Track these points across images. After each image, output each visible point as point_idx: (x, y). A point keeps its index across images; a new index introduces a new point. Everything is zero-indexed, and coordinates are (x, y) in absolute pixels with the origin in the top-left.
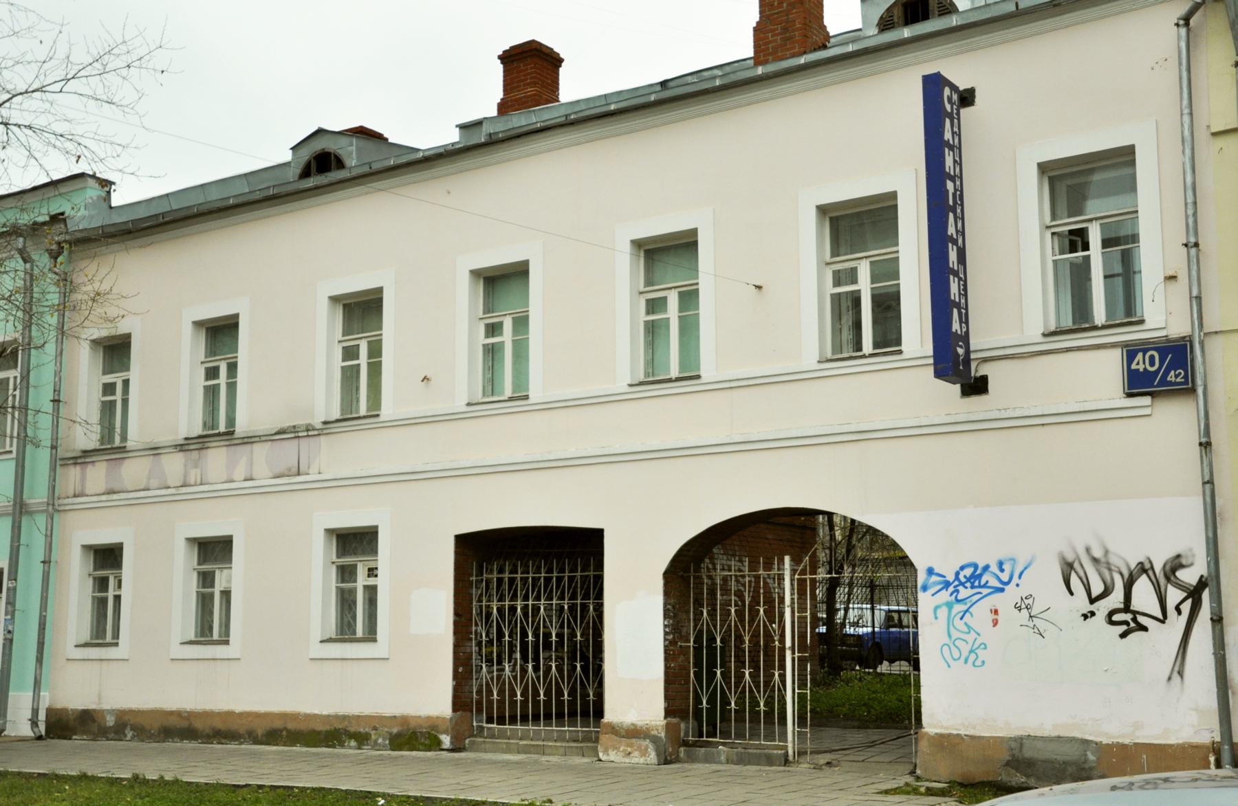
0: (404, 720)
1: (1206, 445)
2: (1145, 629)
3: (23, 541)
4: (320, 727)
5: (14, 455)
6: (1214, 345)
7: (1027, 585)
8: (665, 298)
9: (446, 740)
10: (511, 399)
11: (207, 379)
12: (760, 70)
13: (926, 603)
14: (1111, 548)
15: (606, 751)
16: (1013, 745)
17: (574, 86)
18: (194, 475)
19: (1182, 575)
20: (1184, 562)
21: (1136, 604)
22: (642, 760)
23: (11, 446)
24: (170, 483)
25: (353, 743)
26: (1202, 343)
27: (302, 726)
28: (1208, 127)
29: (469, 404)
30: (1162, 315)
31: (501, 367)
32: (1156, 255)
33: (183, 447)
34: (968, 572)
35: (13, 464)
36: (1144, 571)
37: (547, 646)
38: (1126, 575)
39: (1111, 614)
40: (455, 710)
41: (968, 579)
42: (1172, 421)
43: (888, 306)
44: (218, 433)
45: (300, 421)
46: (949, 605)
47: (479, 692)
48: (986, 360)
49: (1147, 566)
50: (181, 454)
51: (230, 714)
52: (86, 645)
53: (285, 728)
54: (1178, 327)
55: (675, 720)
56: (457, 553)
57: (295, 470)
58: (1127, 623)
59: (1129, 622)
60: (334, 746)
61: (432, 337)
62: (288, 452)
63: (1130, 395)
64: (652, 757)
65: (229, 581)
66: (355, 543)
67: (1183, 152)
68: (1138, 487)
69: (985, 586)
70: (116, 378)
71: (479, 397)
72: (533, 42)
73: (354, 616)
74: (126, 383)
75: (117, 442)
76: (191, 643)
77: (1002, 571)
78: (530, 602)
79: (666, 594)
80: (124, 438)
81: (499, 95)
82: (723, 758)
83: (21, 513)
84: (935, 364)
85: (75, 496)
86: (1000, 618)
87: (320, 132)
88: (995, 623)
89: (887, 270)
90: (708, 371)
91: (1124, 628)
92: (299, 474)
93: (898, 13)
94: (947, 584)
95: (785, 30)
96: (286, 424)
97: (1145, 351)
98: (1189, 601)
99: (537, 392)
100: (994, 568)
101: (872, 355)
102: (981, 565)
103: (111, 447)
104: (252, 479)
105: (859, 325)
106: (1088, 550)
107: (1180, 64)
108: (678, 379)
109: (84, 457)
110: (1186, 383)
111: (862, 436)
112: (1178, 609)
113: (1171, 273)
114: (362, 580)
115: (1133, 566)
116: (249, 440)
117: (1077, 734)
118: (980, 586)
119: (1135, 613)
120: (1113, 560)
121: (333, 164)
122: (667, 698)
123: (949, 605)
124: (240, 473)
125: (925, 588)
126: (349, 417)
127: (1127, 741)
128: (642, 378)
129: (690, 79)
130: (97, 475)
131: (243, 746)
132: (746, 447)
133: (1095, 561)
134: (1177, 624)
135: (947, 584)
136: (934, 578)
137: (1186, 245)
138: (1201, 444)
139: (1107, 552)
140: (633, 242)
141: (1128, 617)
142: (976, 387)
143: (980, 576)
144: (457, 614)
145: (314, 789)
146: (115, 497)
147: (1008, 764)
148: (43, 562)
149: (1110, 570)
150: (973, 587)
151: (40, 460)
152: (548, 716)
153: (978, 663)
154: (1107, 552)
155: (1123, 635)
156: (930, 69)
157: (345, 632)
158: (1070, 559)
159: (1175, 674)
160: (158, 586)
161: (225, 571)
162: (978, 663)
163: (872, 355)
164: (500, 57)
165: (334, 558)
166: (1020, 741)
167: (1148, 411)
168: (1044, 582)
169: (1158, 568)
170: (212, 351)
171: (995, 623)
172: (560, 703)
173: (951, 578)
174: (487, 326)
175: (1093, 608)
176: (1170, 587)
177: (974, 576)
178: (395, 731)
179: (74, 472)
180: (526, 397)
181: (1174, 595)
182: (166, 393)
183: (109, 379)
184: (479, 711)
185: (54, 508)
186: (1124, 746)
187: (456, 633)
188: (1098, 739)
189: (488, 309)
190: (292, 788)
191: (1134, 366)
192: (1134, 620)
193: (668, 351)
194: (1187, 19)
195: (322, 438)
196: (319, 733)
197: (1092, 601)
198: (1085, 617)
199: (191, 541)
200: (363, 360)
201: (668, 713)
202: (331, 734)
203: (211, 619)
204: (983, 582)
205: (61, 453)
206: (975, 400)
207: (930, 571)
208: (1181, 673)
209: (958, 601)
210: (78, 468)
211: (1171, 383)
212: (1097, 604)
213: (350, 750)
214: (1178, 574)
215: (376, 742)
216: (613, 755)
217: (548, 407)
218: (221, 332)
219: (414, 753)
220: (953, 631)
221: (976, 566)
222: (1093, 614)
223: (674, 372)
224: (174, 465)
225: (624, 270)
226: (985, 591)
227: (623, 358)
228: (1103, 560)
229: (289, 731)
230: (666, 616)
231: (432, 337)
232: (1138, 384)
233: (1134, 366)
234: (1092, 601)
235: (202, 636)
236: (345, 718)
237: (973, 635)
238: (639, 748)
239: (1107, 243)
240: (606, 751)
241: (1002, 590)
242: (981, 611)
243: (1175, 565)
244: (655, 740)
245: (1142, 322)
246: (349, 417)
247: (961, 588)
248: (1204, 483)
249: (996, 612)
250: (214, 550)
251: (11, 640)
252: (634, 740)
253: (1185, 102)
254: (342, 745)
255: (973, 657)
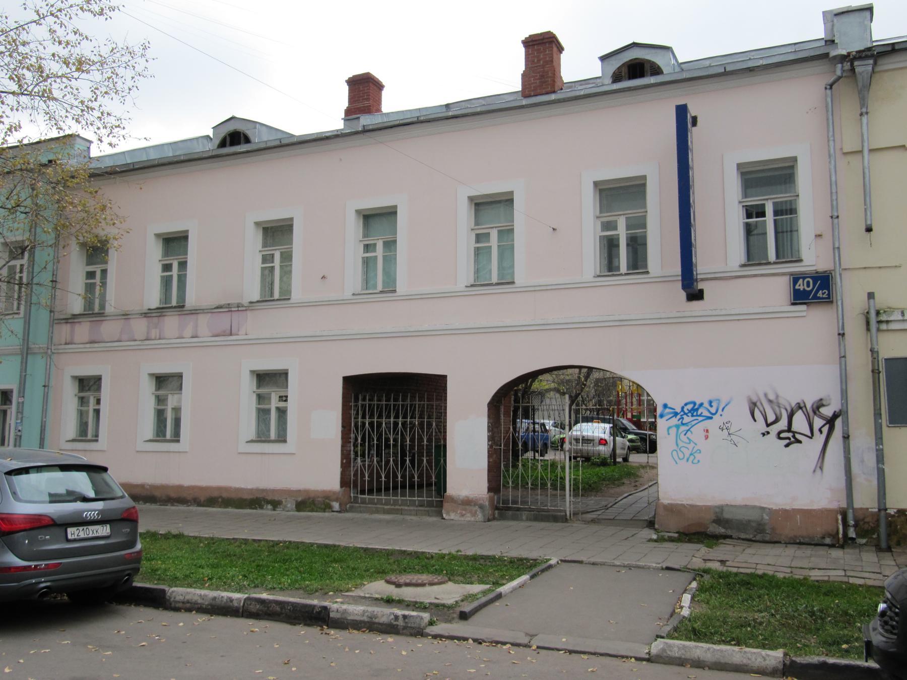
0: (307, 491)
1: (842, 335)
2: (800, 442)
3: (28, 372)
4: (246, 496)
5: (22, 315)
6: (845, 275)
7: (727, 415)
8: (489, 234)
9: (336, 506)
10: (382, 292)
11: (87, 279)
12: (525, 102)
13: (661, 424)
14: (780, 394)
15: (448, 513)
16: (717, 510)
17: (393, 102)
18: (154, 333)
19: (823, 410)
20: (824, 403)
21: (795, 427)
22: (473, 519)
23: (18, 308)
24: (136, 338)
25: (270, 507)
26: (840, 275)
27: (233, 496)
28: (841, 149)
29: (354, 294)
30: (813, 257)
31: (378, 272)
32: (808, 221)
33: (147, 314)
34: (690, 407)
35: (21, 322)
36: (801, 408)
37: (388, 446)
38: (789, 410)
39: (779, 433)
40: (341, 487)
41: (690, 411)
42: (815, 321)
43: (637, 245)
44: (172, 305)
45: (233, 301)
46: (677, 427)
47: (356, 475)
48: (702, 280)
49: (802, 405)
50: (145, 319)
51: (180, 487)
52: (73, 440)
53: (221, 497)
54: (822, 266)
55: (492, 494)
56: (344, 388)
57: (228, 332)
58: (789, 439)
59: (791, 438)
60: (256, 508)
61: (328, 252)
62: (224, 321)
63: (793, 304)
64: (480, 517)
65: (180, 400)
66: (270, 380)
67: (830, 162)
68: (803, 359)
69: (700, 415)
70: (98, 269)
71: (359, 290)
72: (368, 73)
73: (272, 424)
74: (104, 272)
75: (96, 310)
76: (150, 441)
77: (711, 406)
78: (392, 420)
79: (489, 417)
80: (102, 306)
81: (345, 104)
82: (524, 518)
83: (27, 354)
84: (683, 280)
85: (66, 344)
86: (710, 434)
87: (233, 118)
88: (707, 437)
89: (638, 224)
90: (521, 277)
91: (788, 441)
92: (231, 334)
93: (625, 71)
94: (676, 414)
95: (542, 76)
96: (223, 302)
97: (804, 278)
98: (827, 426)
99: (402, 287)
100: (706, 405)
101: (626, 274)
102: (698, 403)
103: (94, 312)
104: (197, 337)
105: (624, 254)
106: (766, 395)
107: (827, 111)
108: (498, 284)
109: (73, 319)
110: (829, 298)
111: (622, 323)
112: (820, 431)
113: (819, 233)
114: (274, 403)
115: (793, 405)
116: (195, 312)
117: (757, 504)
118: (697, 415)
119: (794, 433)
120: (781, 401)
121: (242, 139)
122: (489, 481)
123: (677, 427)
124: (188, 332)
125: (662, 416)
126: (267, 298)
127: (788, 508)
128: (598, 273)
129: (751, 56)
130: (83, 330)
131: (191, 508)
132: (545, 327)
133: (770, 401)
134: (820, 439)
135: (676, 414)
136: (667, 410)
137: (832, 217)
138: (839, 334)
139: (777, 397)
140: (357, 211)
141: (790, 435)
142: (695, 295)
143: (697, 410)
144: (343, 426)
145: (320, 546)
146: (96, 345)
147: (714, 521)
148: (44, 386)
149: (779, 407)
150: (692, 416)
151: (41, 318)
152: (387, 489)
153: (696, 461)
154: (777, 397)
155: (787, 446)
156: (681, 102)
157: (262, 437)
158: (755, 399)
159: (818, 468)
160: (128, 407)
161: (176, 396)
162: (696, 461)
163: (626, 274)
164: (347, 81)
165: (255, 389)
166: (721, 508)
167: (804, 314)
168: (738, 414)
169: (809, 406)
170: (167, 252)
171: (707, 437)
172: (379, 482)
173: (678, 410)
174: (602, 223)
175: (768, 429)
176: (816, 418)
177: (694, 409)
178: (300, 499)
179: (65, 329)
180: (395, 291)
181: (818, 423)
182: (135, 277)
183: (91, 268)
184: (355, 486)
185: (49, 353)
186: (786, 511)
187: (342, 438)
188: (770, 507)
189: (365, 235)
190: (260, 541)
191: (797, 287)
192: (794, 437)
193: (493, 268)
194: (831, 86)
195: (248, 312)
196: (246, 500)
197: (768, 425)
198: (764, 434)
199: (151, 375)
200: (175, 272)
201: (490, 489)
202: (255, 501)
203: (167, 427)
204: (699, 413)
205: (57, 316)
206: (695, 304)
207: (665, 406)
208: (821, 468)
209: (683, 424)
210: (69, 325)
211: (819, 298)
212: (771, 427)
213: (268, 510)
214: (821, 410)
215: (285, 506)
216: (453, 516)
217: (409, 298)
218: (175, 243)
219: (315, 514)
220: (679, 441)
221: (695, 404)
222: (768, 433)
223: (495, 280)
224: (140, 326)
225: (353, 228)
226: (700, 418)
227: (351, 278)
228: (775, 401)
229: (223, 499)
230: (489, 431)
231: (328, 252)
232: (799, 297)
233: (797, 287)
234: (768, 425)
235: (81, 435)
236: (263, 490)
237: (692, 445)
238: (471, 512)
239: (776, 213)
240: (448, 513)
241: (711, 418)
242: (698, 431)
243: (819, 405)
244: (481, 507)
245: (800, 261)
246: (267, 298)
247: (685, 416)
248: (841, 357)
249: (707, 431)
250: (165, 382)
251: (20, 436)
252: (467, 507)
253: (831, 134)
254: (261, 507)
255: (692, 457)
